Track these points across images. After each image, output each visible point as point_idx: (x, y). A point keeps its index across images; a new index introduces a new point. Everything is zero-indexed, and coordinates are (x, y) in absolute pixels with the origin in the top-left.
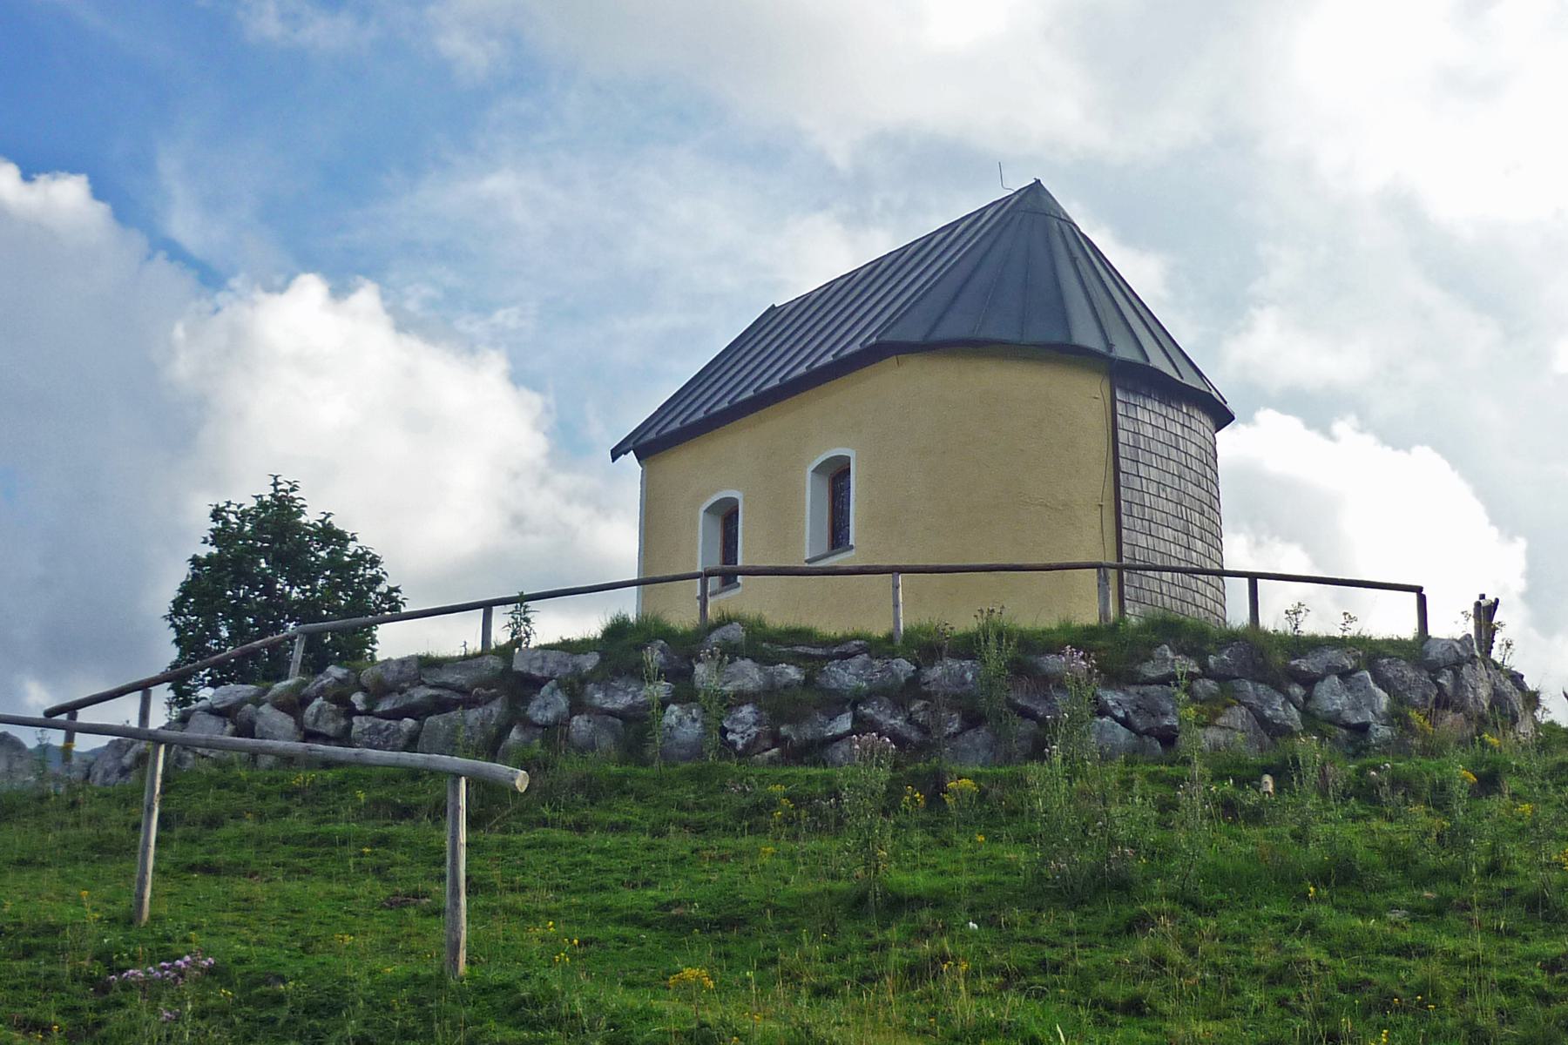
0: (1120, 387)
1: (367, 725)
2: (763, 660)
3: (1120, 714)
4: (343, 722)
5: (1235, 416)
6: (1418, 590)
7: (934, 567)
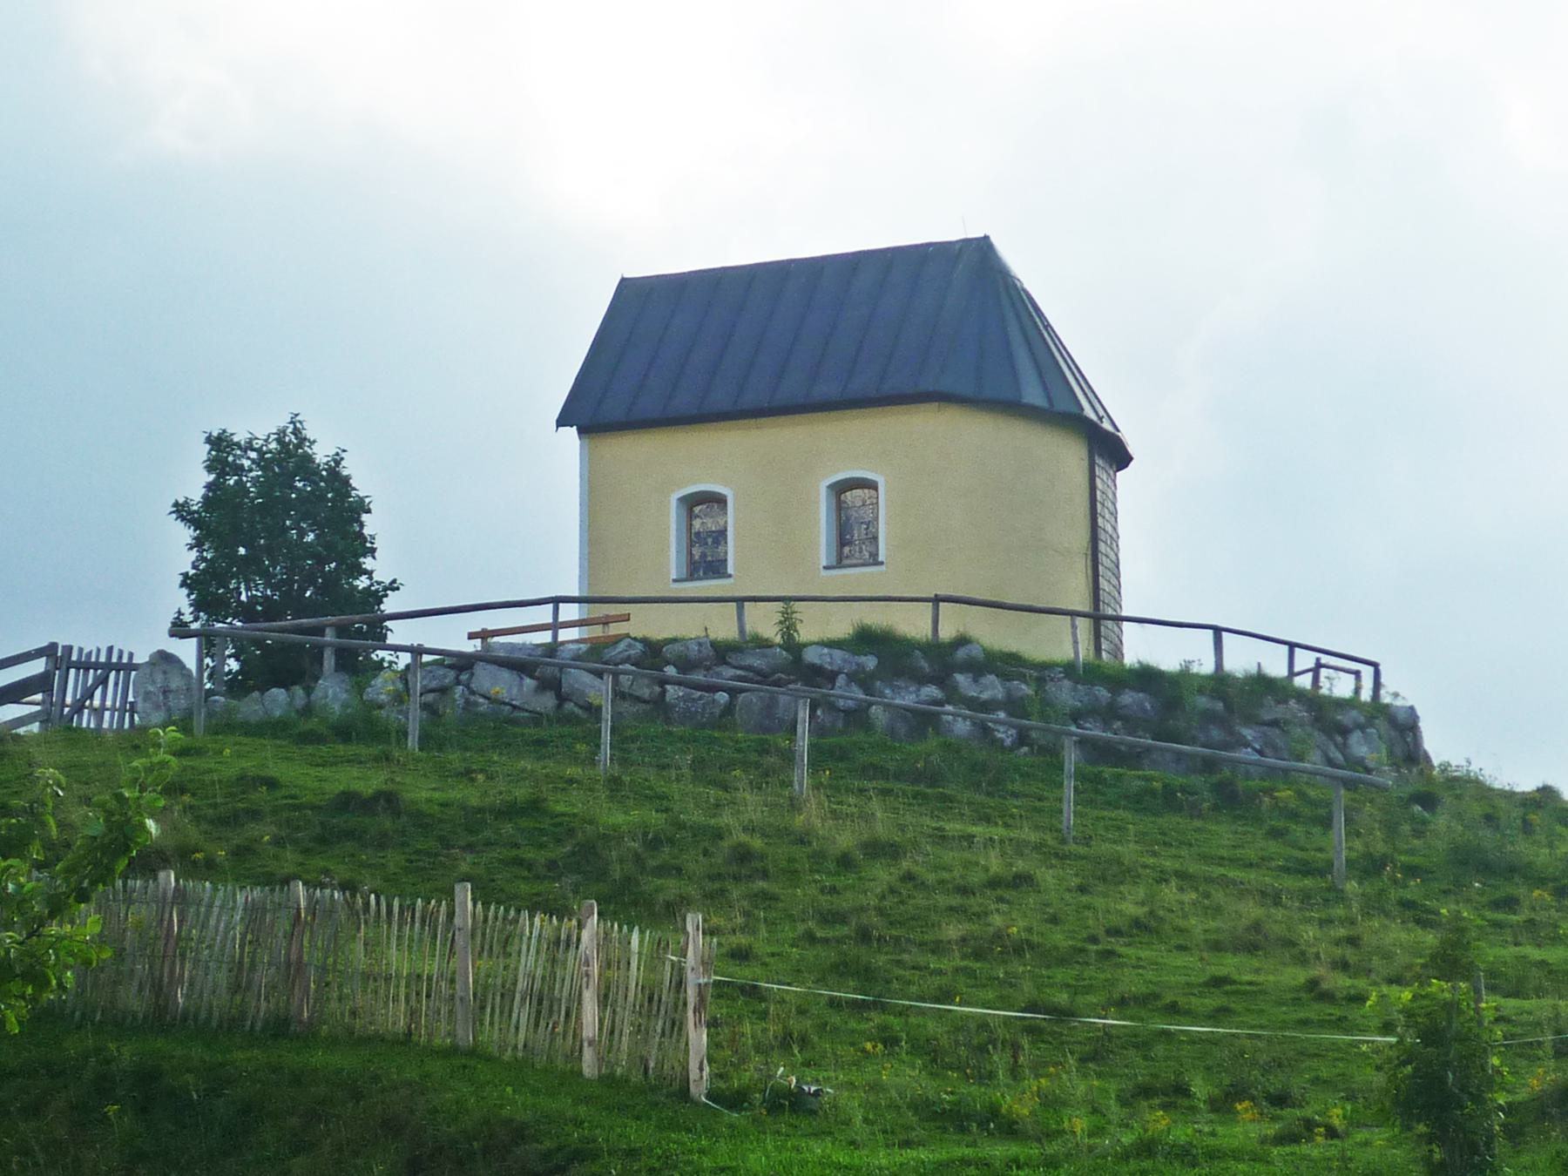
0: (1101, 455)
1: (681, 694)
2: (1005, 677)
3: (1258, 747)
4: (658, 689)
5: (55, 641)
6: (1375, 665)
7: (659, 598)
